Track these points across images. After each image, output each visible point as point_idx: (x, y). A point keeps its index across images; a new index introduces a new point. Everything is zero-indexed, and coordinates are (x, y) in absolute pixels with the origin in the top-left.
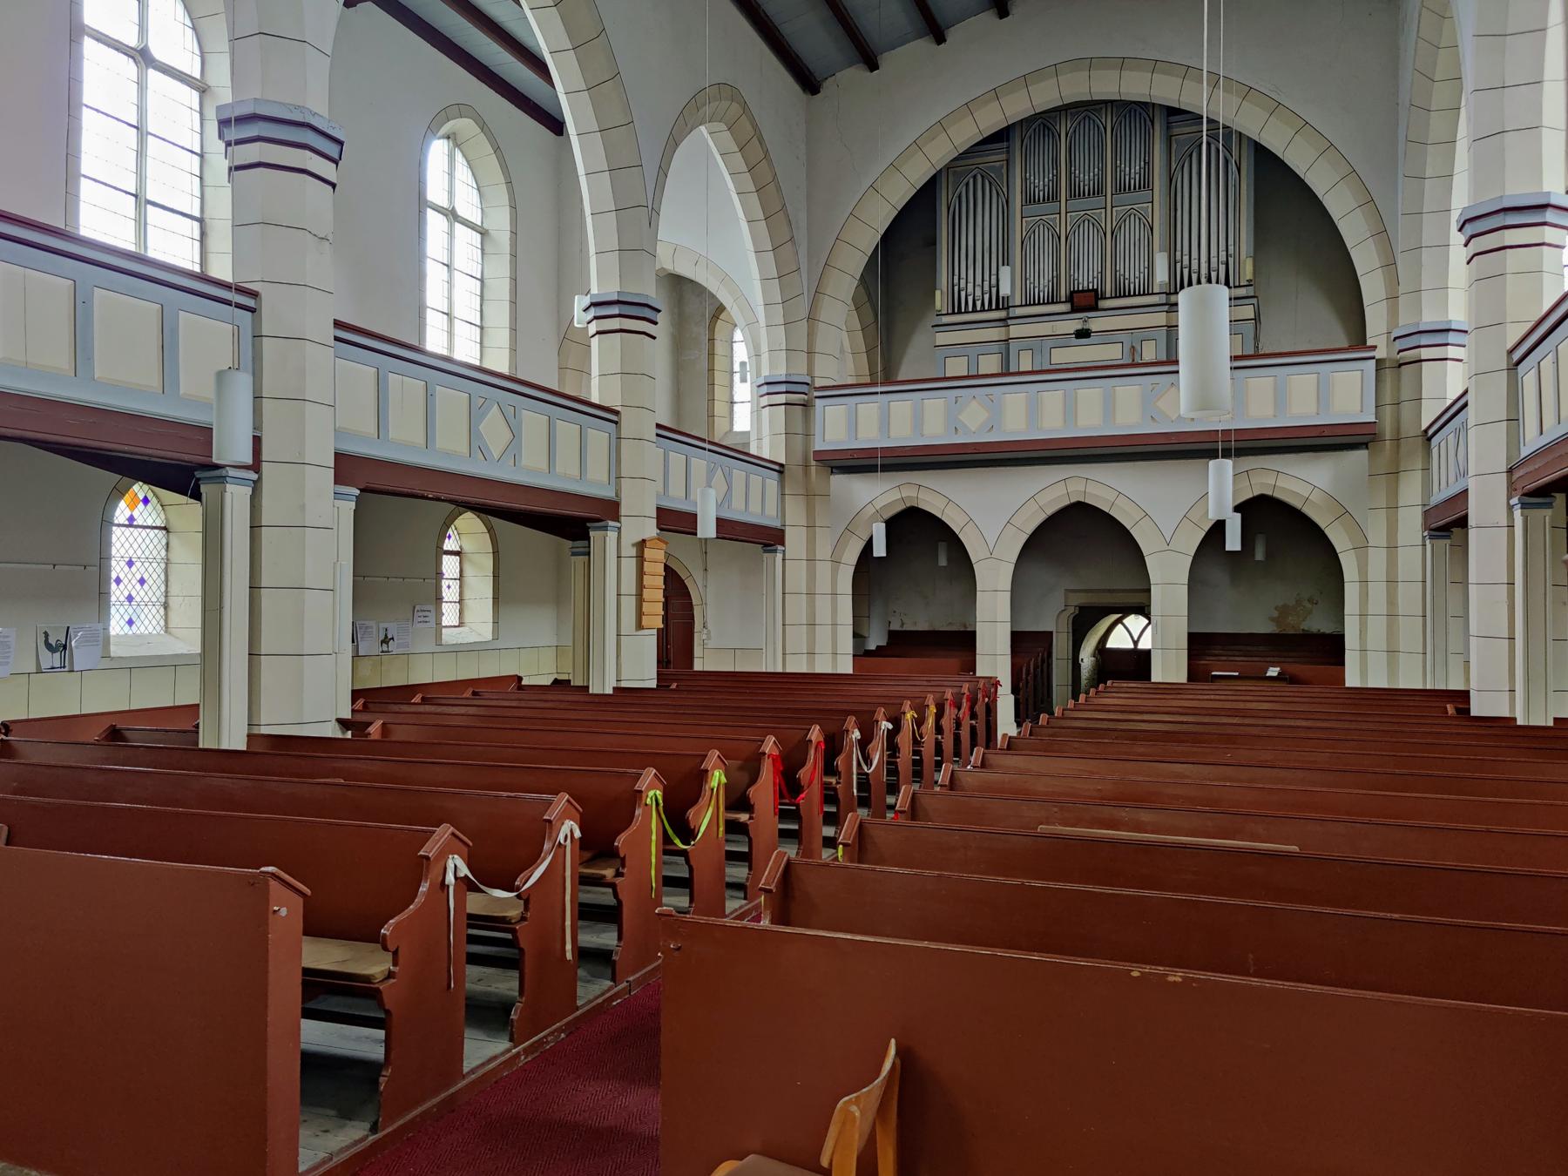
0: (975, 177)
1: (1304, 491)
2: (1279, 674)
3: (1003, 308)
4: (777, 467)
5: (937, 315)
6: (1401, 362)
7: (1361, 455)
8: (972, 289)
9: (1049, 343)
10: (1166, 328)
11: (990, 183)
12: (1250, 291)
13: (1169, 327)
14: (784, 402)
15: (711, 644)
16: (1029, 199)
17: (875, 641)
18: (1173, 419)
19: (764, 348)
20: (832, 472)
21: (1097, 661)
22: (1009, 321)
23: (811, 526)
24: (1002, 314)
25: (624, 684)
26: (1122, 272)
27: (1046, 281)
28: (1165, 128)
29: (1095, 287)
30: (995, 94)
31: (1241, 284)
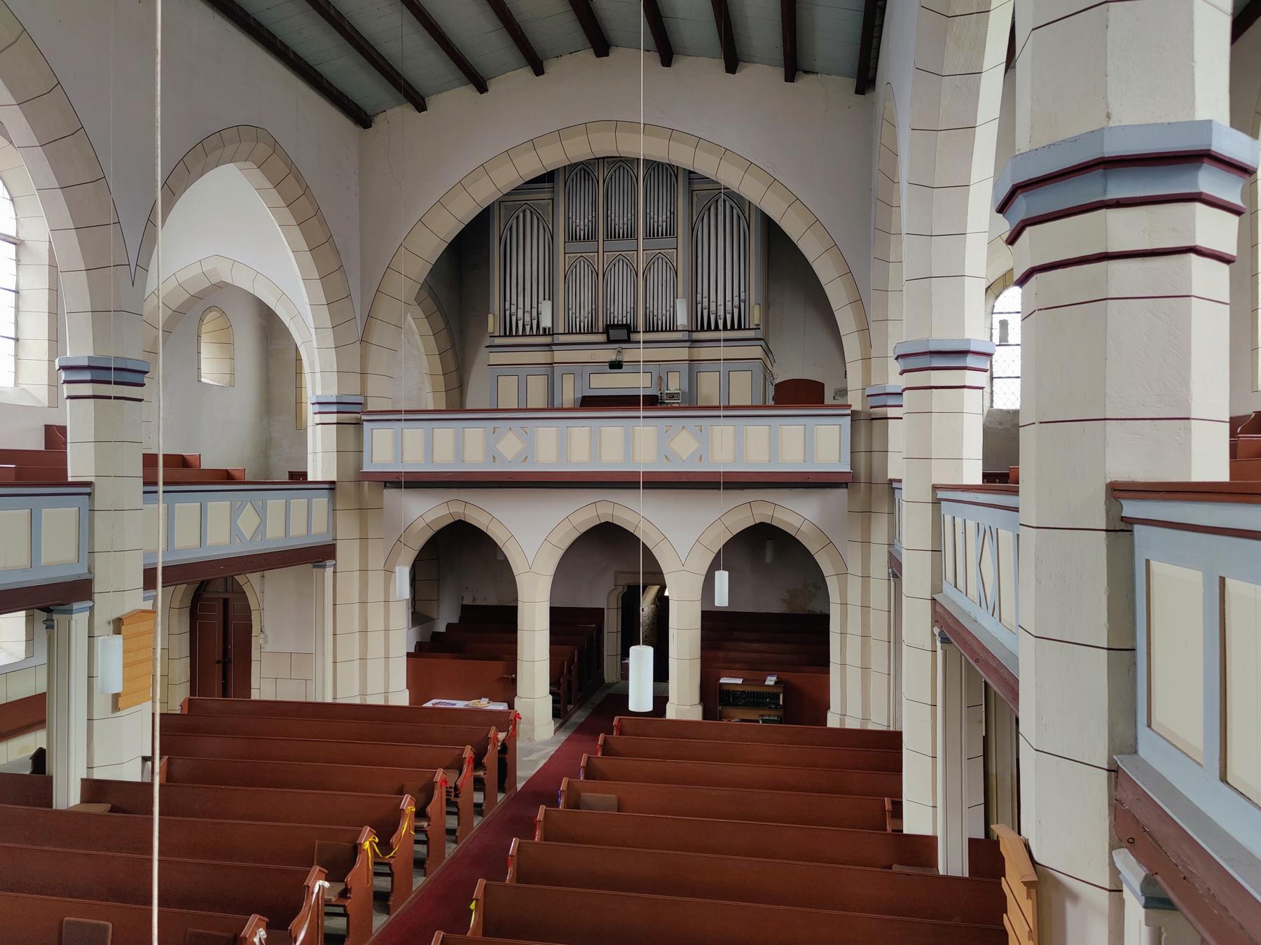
2: (776, 683)
3: (549, 335)
4: (327, 486)
5: (490, 337)
6: (873, 417)
7: (842, 492)
8: (521, 315)
9: (588, 369)
10: (688, 362)
12: (759, 334)
14: (335, 421)
15: (268, 648)
16: (572, 237)
17: (445, 618)
18: (684, 458)
19: (318, 369)
20: (385, 486)
21: (657, 606)
22: (553, 347)
23: (364, 539)
24: (547, 340)
25: (98, 775)
26: (651, 310)
27: (586, 313)
28: (687, 184)
29: (629, 322)
30: (533, 144)
31: (751, 327)
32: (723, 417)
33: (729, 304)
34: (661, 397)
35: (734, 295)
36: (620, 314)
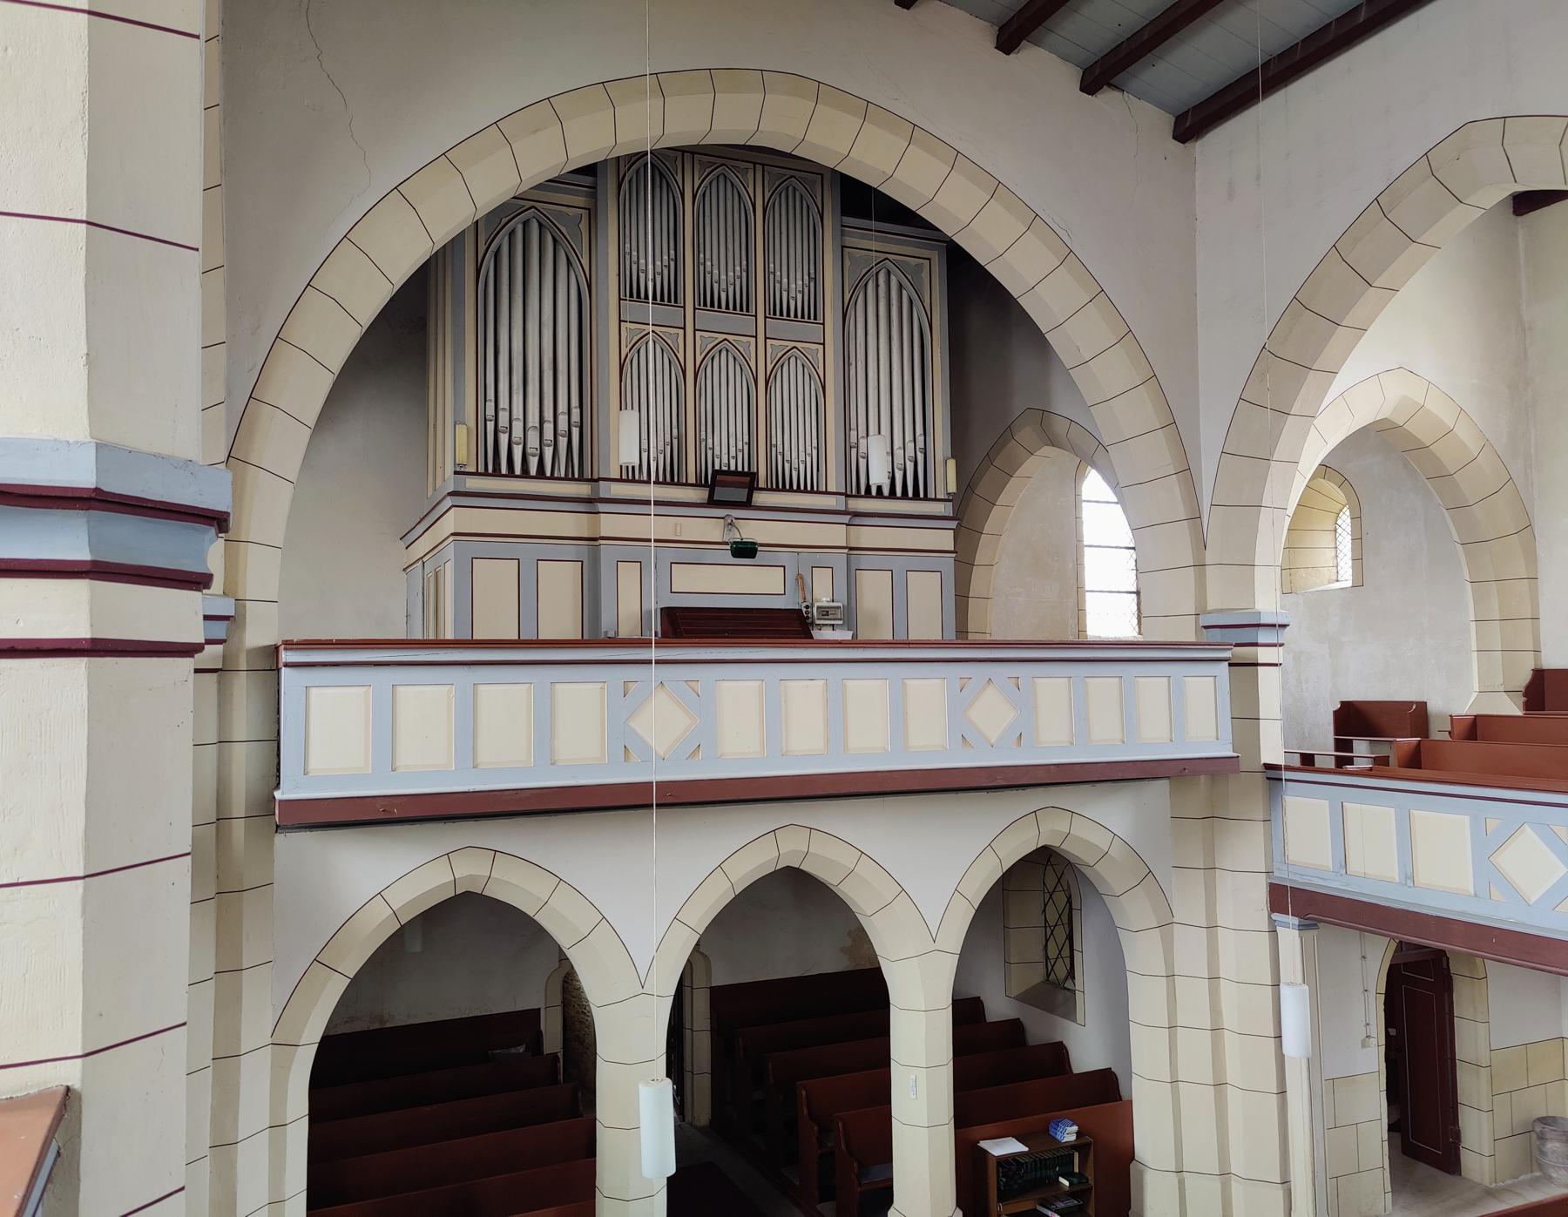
0: (526, 224)
1: (1100, 840)
10: (846, 551)
11: (555, 241)
13: (851, 549)
16: (632, 292)
24: (583, 490)
26: (780, 450)
31: (938, 497)
32: (658, 662)
33: (563, 420)
34: (807, 612)
35: (907, 440)
36: (727, 451)
